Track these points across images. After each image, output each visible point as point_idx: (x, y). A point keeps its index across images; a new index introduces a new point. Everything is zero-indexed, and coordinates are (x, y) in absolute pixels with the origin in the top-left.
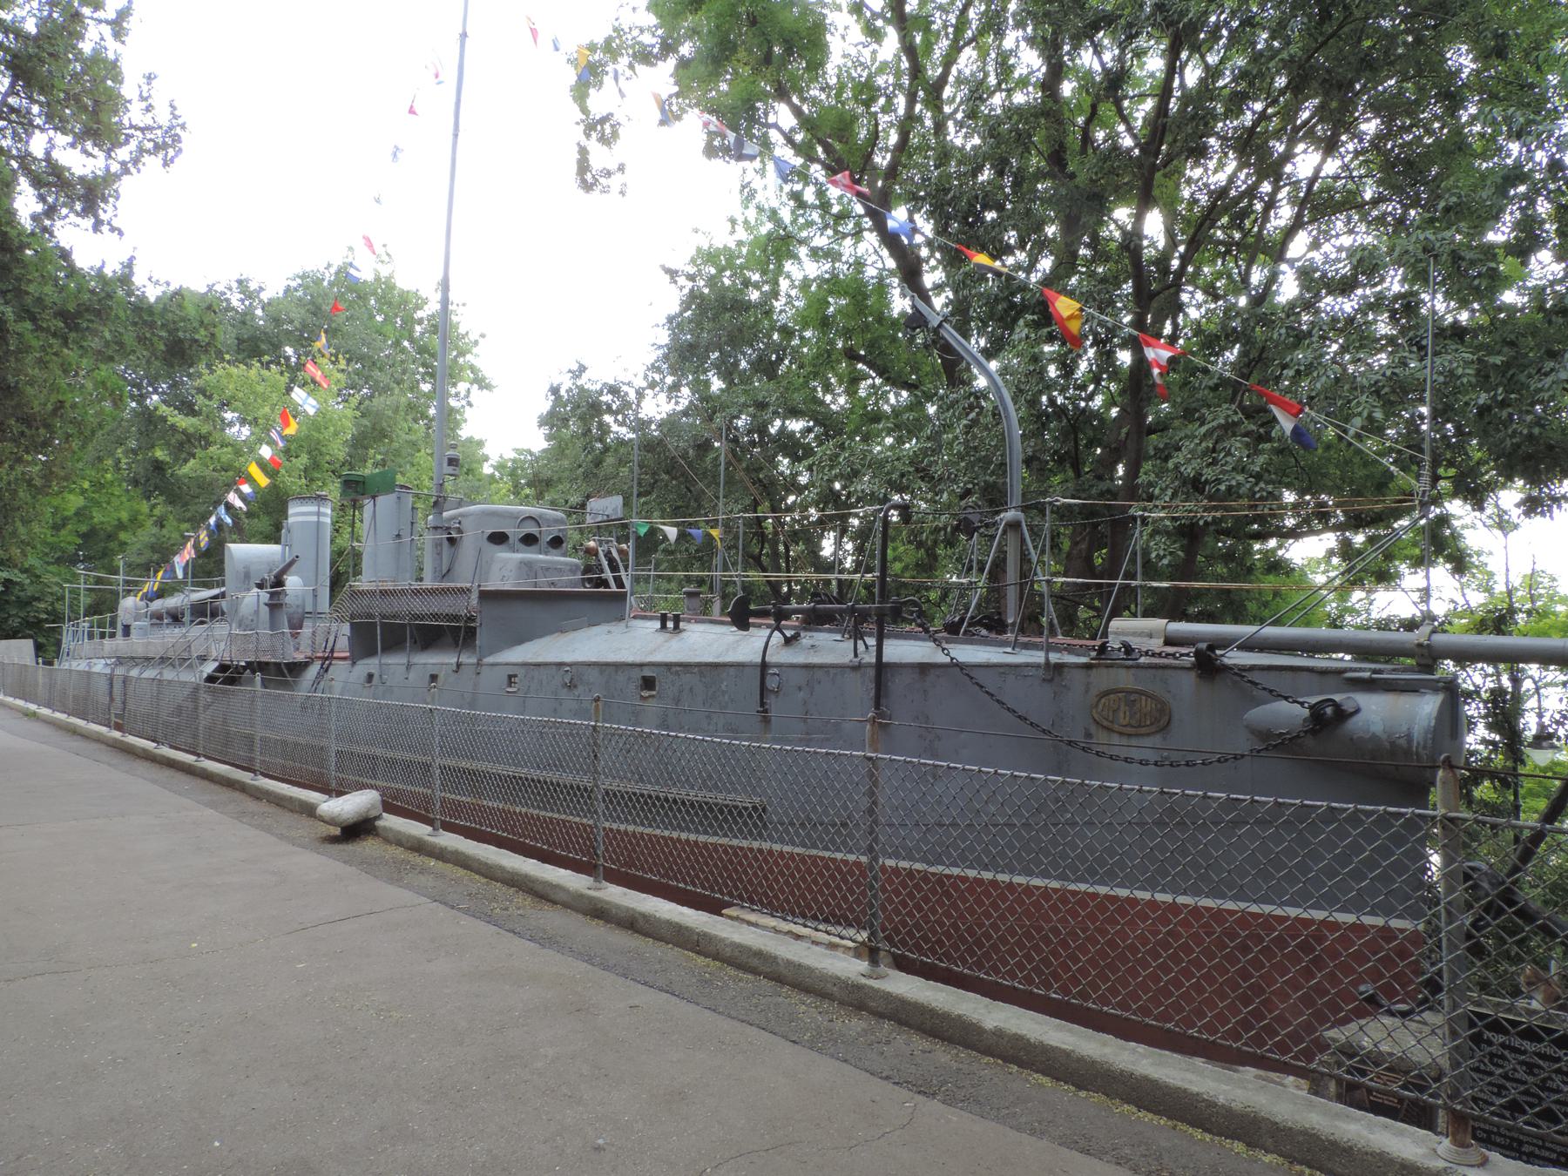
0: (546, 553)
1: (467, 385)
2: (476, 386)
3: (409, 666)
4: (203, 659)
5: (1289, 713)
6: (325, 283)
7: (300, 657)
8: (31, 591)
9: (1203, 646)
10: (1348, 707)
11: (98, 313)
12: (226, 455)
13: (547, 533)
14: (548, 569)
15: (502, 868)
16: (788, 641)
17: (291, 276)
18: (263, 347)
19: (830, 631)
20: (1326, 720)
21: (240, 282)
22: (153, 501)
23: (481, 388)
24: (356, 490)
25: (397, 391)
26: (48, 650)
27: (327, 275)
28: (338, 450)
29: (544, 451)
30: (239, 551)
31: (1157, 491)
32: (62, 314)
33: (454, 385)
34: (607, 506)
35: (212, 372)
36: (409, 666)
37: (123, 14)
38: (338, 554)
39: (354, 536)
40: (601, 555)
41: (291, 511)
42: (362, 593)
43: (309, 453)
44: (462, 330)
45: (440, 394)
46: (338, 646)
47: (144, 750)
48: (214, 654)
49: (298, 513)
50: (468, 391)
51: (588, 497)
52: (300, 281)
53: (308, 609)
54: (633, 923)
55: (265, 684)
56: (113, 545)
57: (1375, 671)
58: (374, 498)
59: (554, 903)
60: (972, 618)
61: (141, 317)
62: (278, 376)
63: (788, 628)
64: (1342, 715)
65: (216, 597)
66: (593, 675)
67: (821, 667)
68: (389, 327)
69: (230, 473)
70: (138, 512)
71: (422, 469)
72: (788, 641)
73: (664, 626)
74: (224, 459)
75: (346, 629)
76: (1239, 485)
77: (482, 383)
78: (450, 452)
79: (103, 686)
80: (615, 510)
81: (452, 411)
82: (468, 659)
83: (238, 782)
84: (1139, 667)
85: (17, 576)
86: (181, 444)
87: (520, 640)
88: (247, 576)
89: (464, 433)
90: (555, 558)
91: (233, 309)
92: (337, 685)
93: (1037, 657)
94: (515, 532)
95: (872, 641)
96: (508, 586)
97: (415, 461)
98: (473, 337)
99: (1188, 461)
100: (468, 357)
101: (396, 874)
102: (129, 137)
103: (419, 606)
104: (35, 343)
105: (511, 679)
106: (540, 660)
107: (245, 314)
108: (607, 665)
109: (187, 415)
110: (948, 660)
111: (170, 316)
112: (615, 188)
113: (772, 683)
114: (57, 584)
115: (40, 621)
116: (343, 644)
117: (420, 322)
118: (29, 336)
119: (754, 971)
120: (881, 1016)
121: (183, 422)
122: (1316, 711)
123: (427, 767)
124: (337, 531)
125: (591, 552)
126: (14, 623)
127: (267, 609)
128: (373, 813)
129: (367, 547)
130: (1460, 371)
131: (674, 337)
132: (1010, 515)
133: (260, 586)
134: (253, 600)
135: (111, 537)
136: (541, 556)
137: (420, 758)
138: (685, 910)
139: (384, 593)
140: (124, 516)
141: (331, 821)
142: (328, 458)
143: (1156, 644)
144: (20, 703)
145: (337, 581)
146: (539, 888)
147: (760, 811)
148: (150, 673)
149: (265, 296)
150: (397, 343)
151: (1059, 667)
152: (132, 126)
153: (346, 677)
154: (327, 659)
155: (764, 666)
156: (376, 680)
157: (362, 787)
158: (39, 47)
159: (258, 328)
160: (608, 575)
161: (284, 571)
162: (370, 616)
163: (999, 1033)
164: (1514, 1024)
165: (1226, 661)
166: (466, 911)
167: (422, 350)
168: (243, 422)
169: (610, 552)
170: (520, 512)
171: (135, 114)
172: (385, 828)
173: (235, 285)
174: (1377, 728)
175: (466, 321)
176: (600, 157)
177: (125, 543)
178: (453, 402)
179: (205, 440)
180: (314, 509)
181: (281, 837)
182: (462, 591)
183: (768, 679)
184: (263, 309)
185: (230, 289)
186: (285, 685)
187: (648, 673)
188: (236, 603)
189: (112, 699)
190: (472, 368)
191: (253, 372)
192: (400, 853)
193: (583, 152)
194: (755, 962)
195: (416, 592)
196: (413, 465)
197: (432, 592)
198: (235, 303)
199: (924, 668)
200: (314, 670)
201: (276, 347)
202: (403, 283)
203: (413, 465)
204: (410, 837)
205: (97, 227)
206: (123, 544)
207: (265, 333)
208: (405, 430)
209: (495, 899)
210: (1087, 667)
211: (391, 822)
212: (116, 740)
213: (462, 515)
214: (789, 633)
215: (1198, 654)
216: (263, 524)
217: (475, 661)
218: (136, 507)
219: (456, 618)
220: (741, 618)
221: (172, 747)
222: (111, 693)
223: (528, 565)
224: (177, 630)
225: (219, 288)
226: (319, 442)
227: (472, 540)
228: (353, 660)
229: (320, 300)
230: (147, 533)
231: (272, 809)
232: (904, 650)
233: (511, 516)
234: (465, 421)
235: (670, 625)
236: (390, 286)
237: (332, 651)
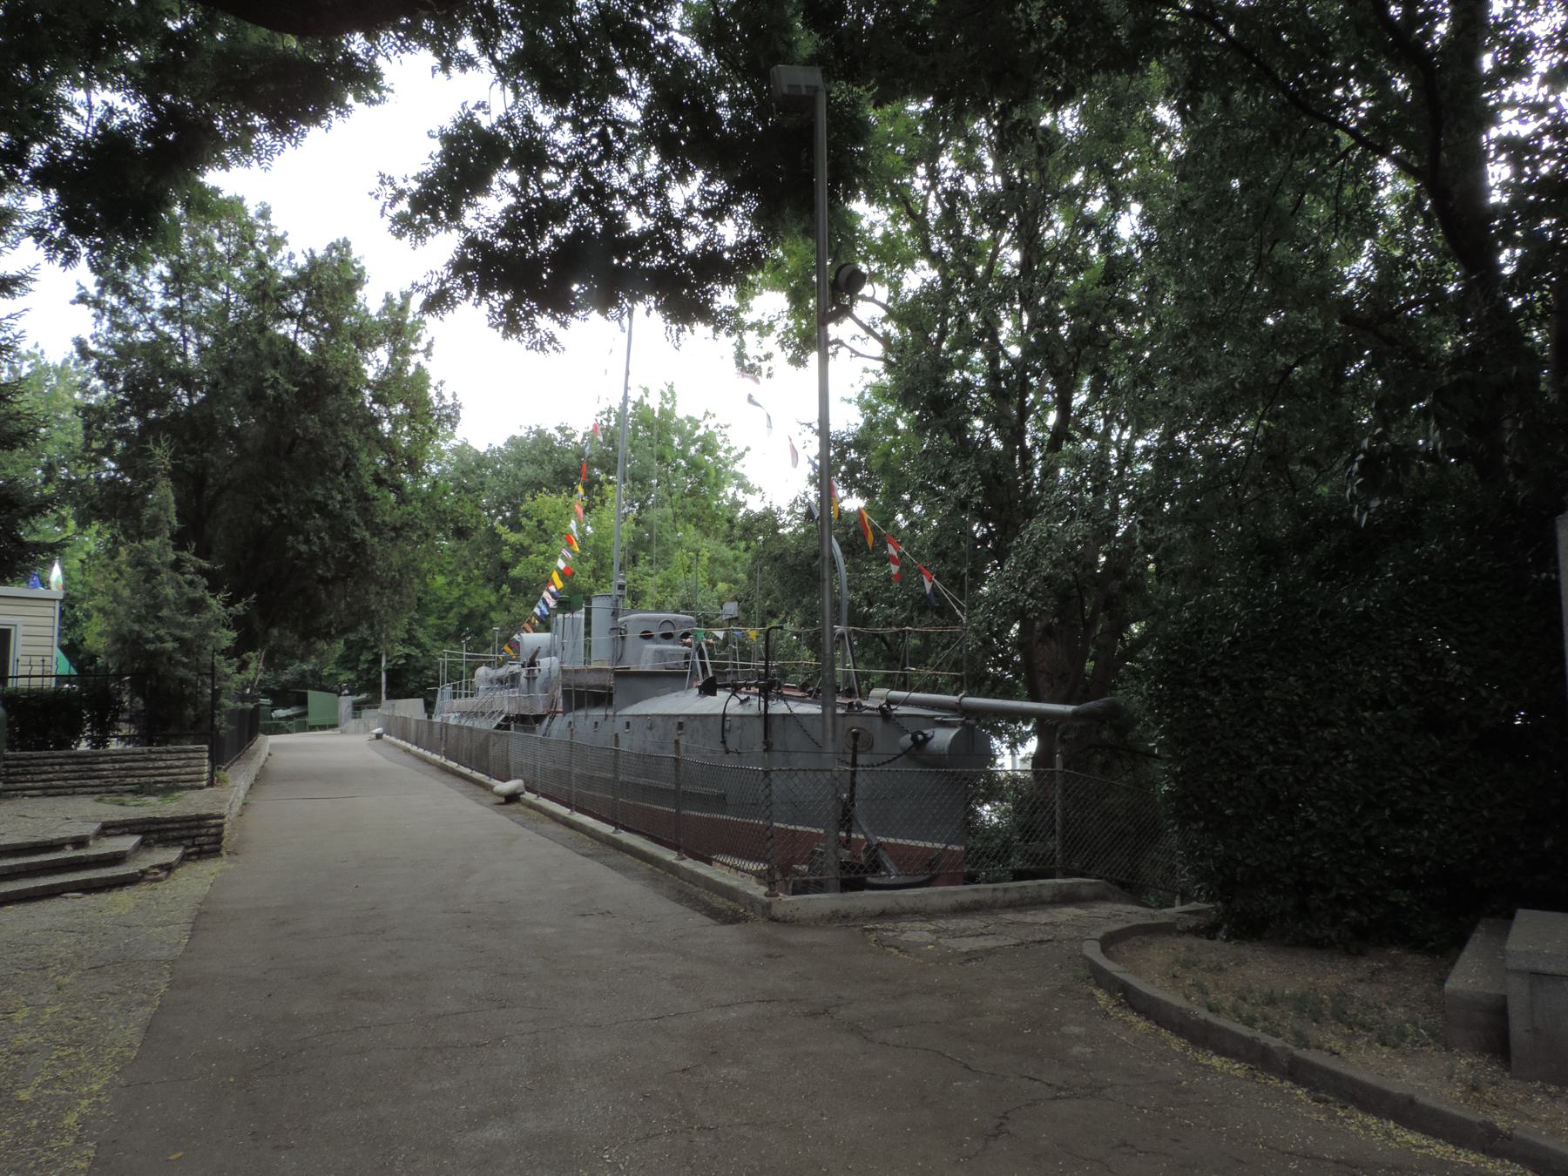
3: (586, 716)
8: (423, 662)
11: (411, 527)
13: (679, 631)
20: (920, 743)
32: (394, 529)
35: (534, 499)
56: (486, 623)
66: (659, 721)
72: (742, 702)
74: (539, 564)
82: (610, 713)
85: (415, 652)
87: (636, 701)
90: (668, 647)
94: (657, 633)
113: (727, 726)
126: (412, 686)
141: (499, 794)
144: (403, 743)
147: (723, 797)
155: (724, 715)
157: (516, 778)
199: (784, 716)
219: (604, 687)
223: (660, 653)
227: (633, 635)
232: (778, 708)
233: (655, 620)
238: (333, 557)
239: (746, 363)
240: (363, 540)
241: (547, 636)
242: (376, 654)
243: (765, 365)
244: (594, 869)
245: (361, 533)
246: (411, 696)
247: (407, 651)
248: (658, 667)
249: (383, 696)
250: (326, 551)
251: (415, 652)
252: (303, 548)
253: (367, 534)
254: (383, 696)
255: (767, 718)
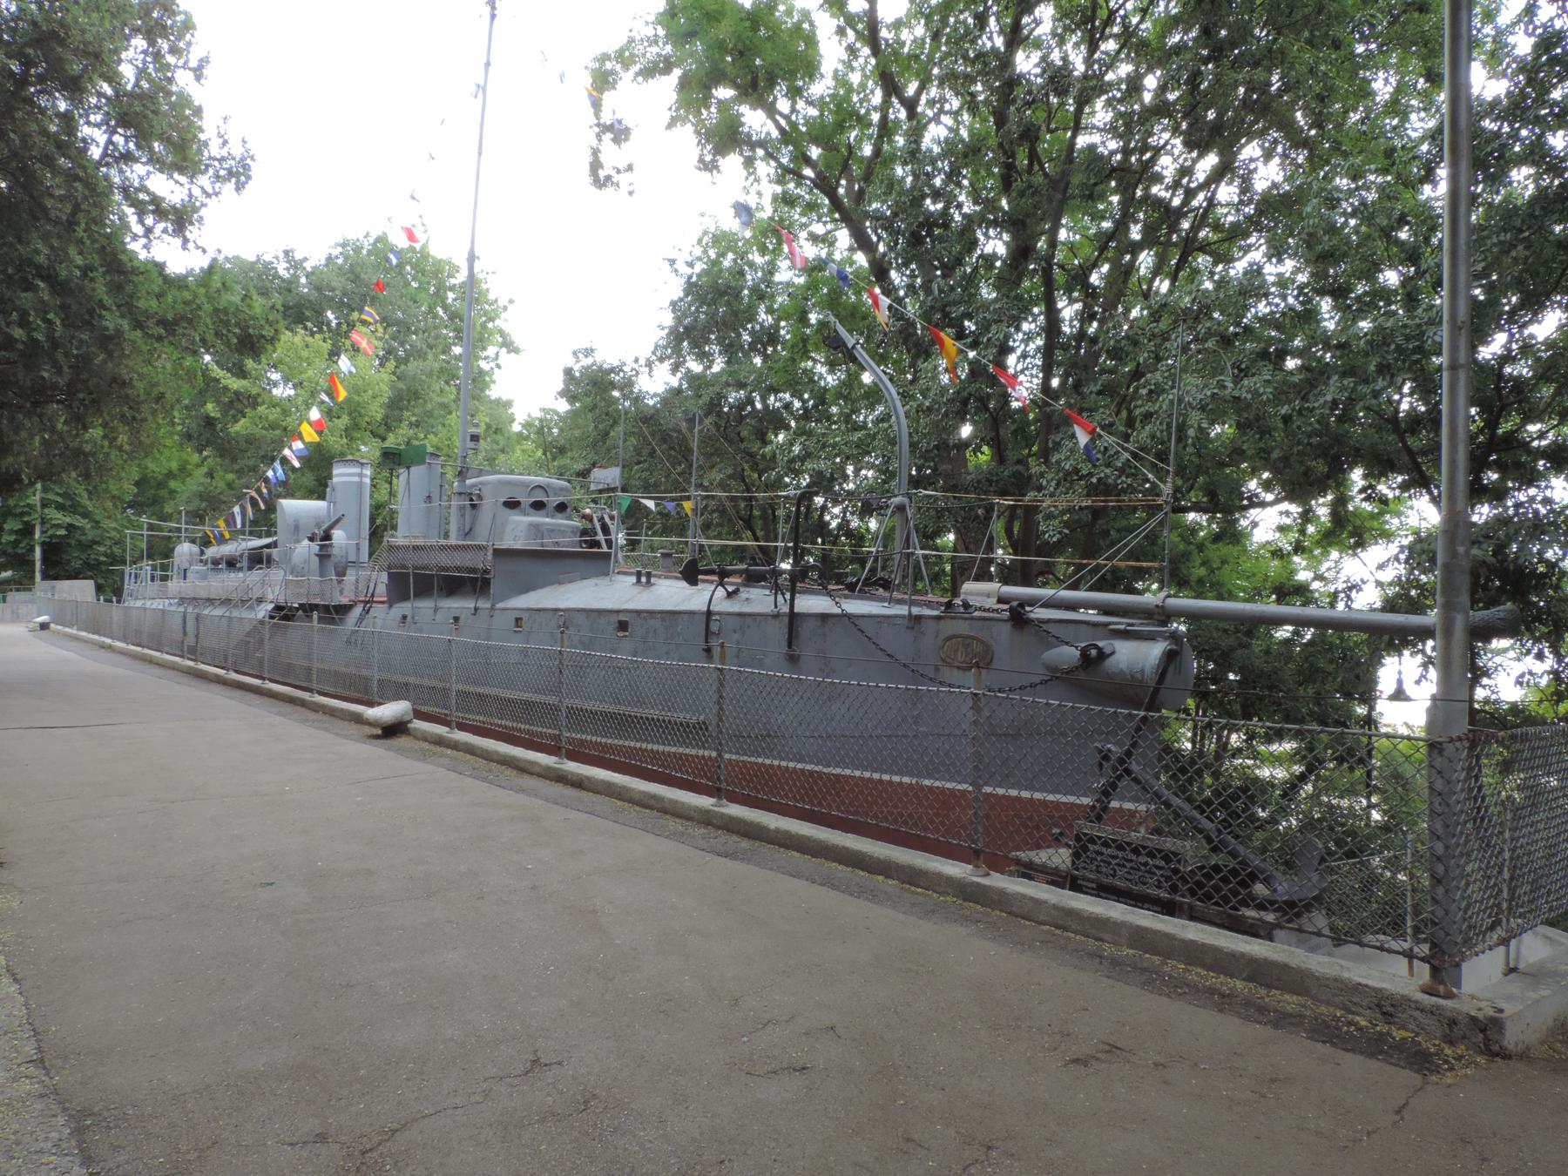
0: (552, 517)
1: (496, 349)
2: (504, 350)
3: (436, 610)
4: (260, 601)
5: (1069, 654)
6: (364, 252)
7: (345, 601)
8: (92, 535)
9: (1015, 604)
10: (1107, 651)
11: (190, 321)
12: (274, 414)
13: (554, 501)
14: (553, 531)
15: (497, 753)
16: (730, 595)
17: (333, 244)
18: (307, 313)
19: (763, 587)
20: (1092, 660)
21: (286, 253)
22: (205, 453)
23: (509, 352)
24: (392, 460)
25: (430, 356)
26: (111, 589)
27: (366, 243)
28: (376, 412)
29: (567, 412)
30: (291, 506)
31: (1044, 483)
32: (162, 322)
33: (484, 349)
34: (609, 475)
36: (436, 610)
37: (203, 62)
38: (377, 508)
39: (392, 494)
40: (595, 520)
41: (335, 472)
42: (398, 548)
43: (350, 414)
44: (491, 297)
45: (471, 355)
46: (377, 591)
47: (217, 675)
48: (270, 596)
49: (342, 474)
50: (497, 353)
51: (594, 465)
52: (340, 249)
53: (352, 558)
54: (579, 783)
55: (320, 620)
56: (163, 493)
57: (1132, 625)
58: (408, 468)
59: (532, 774)
60: (866, 579)
61: (218, 317)
62: (321, 343)
63: (731, 584)
64: (1102, 656)
65: (268, 546)
66: (580, 619)
67: (750, 615)
68: (423, 295)
69: (278, 432)
70: (186, 462)
71: (451, 432)
72: (730, 595)
73: (639, 581)
74: (271, 417)
75: (384, 577)
76: (1107, 476)
77: (509, 345)
78: (473, 430)
79: (178, 620)
80: (614, 479)
81: (481, 372)
82: (483, 604)
83: (298, 698)
84: (972, 618)
85: (79, 521)
86: (231, 402)
87: (526, 589)
88: (297, 528)
89: (494, 392)
90: (561, 521)
91: (280, 277)
92: (379, 622)
93: (902, 610)
94: (526, 500)
95: (788, 596)
96: (519, 546)
97: (447, 422)
98: (501, 303)
99: (1067, 458)
100: (497, 322)
101: (423, 756)
102: (207, 166)
103: (445, 560)
104: (145, 348)
105: (518, 621)
106: (540, 606)
107: (290, 282)
108: (592, 611)
109: (238, 377)
110: (839, 611)
111: (241, 316)
112: (624, 188)
113: (714, 627)
114: (115, 529)
115: (100, 563)
116: (382, 589)
117: (452, 288)
118: (140, 342)
119: (651, 808)
120: (718, 827)
121: (235, 384)
122: (1084, 653)
123: (446, 691)
124: (375, 486)
125: (589, 518)
126: (77, 564)
127: (317, 559)
128: (406, 718)
129: (401, 506)
130: (1261, 390)
131: (679, 320)
132: (897, 500)
133: (311, 539)
134: (305, 549)
135: (161, 485)
136: (547, 520)
137: (440, 685)
138: (616, 775)
139: (416, 548)
140: (174, 465)
142: (366, 419)
143: (991, 602)
144: (96, 637)
145: (376, 534)
146: (521, 765)
148: (218, 612)
149: (308, 266)
150: (431, 310)
151: (919, 618)
152: (210, 158)
153: (384, 618)
154: (368, 602)
155: (709, 613)
156: (409, 619)
158: (144, 105)
159: (302, 296)
160: (601, 537)
161: (332, 526)
162: (404, 567)
163: (777, 830)
164: (1100, 838)
165: (1032, 616)
166: (470, 776)
167: (454, 316)
168: (286, 380)
169: (603, 518)
170: (532, 481)
171: (215, 150)
172: (415, 729)
173: (281, 255)
174: (1123, 666)
175: (496, 289)
176: (612, 156)
177: (175, 491)
178: (483, 365)
179: (254, 402)
180: (357, 470)
181: (337, 735)
182: (479, 548)
183: (712, 623)
184: (307, 277)
185: (277, 258)
186: (332, 621)
187: (623, 618)
188: (288, 555)
189: (185, 633)
190: (501, 332)
191: (297, 339)
192: (426, 745)
193: (595, 152)
194: (652, 802)
195: (443, 548)
196: (444, 425)
197: (456, 548)
198: (283, 273)
199: (824, 617)
200: (357, 611)
201: (319, 313)
202: (438, 251)
203: (444, 425)
204: (433, 734)
205: (184, 246)
206: (172, 492)
207: (309, 301)
208: (439, 392)
209: (490, 771)
210: (938, 618)
211: (419, 725)
212: (190, 667)
213: (481, 483)
214: (730, 589)
215: (1011, 609)
216: (309, 479)
217: (489, 606)
218: (185, 457)
219: (474, 570)
220: (691, 575)
221: (237, 672)
222: (184, 628)
223: (535, 527)
224: (232, 575)
225: (268, 258)
226: (358, 404)
227: (489, 505)
228: (390, 603)
229: (359, 269)
230: (196, 481)
231: (327, 718)
232: (812, 603)
233: (524, 485)
234: (494, 382)
235: (644, 579)
236: (425, 256)
237: (373, 596)
238: (67, 355)
239: (602, 174)
240: (119, 332)
241: (321, 504)
242: (26, 523)
243: (623, 179)
244: (828, 899)
245: (112, 321)
246: (75, 575)
247: (68, 520)
248: (534, 546)
249: (38, 576)
250: (55, 344)
251: (79, 521)
252: (18, 333)
253: (125, 324)
254: (38, 576)
255: (793, 617)
